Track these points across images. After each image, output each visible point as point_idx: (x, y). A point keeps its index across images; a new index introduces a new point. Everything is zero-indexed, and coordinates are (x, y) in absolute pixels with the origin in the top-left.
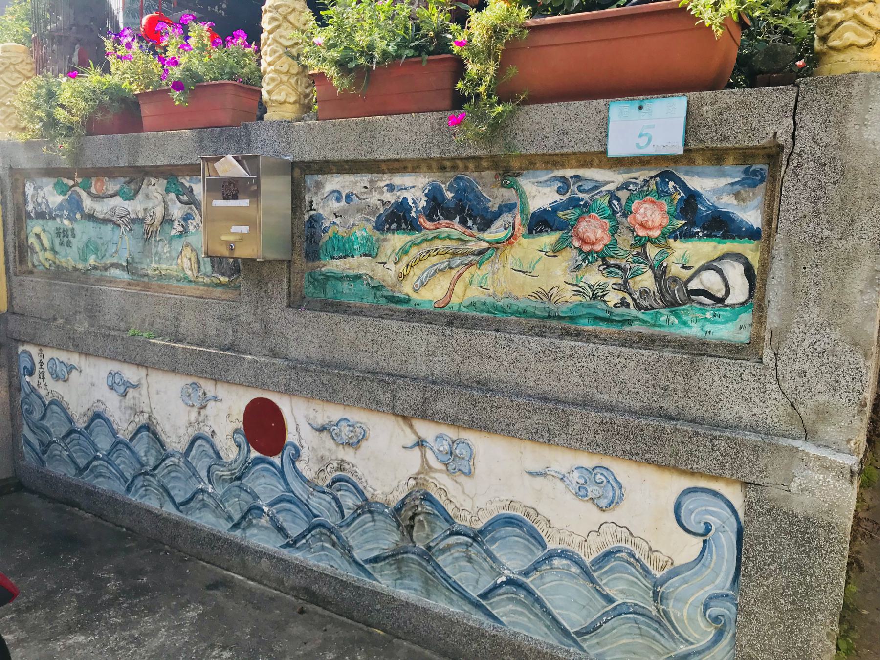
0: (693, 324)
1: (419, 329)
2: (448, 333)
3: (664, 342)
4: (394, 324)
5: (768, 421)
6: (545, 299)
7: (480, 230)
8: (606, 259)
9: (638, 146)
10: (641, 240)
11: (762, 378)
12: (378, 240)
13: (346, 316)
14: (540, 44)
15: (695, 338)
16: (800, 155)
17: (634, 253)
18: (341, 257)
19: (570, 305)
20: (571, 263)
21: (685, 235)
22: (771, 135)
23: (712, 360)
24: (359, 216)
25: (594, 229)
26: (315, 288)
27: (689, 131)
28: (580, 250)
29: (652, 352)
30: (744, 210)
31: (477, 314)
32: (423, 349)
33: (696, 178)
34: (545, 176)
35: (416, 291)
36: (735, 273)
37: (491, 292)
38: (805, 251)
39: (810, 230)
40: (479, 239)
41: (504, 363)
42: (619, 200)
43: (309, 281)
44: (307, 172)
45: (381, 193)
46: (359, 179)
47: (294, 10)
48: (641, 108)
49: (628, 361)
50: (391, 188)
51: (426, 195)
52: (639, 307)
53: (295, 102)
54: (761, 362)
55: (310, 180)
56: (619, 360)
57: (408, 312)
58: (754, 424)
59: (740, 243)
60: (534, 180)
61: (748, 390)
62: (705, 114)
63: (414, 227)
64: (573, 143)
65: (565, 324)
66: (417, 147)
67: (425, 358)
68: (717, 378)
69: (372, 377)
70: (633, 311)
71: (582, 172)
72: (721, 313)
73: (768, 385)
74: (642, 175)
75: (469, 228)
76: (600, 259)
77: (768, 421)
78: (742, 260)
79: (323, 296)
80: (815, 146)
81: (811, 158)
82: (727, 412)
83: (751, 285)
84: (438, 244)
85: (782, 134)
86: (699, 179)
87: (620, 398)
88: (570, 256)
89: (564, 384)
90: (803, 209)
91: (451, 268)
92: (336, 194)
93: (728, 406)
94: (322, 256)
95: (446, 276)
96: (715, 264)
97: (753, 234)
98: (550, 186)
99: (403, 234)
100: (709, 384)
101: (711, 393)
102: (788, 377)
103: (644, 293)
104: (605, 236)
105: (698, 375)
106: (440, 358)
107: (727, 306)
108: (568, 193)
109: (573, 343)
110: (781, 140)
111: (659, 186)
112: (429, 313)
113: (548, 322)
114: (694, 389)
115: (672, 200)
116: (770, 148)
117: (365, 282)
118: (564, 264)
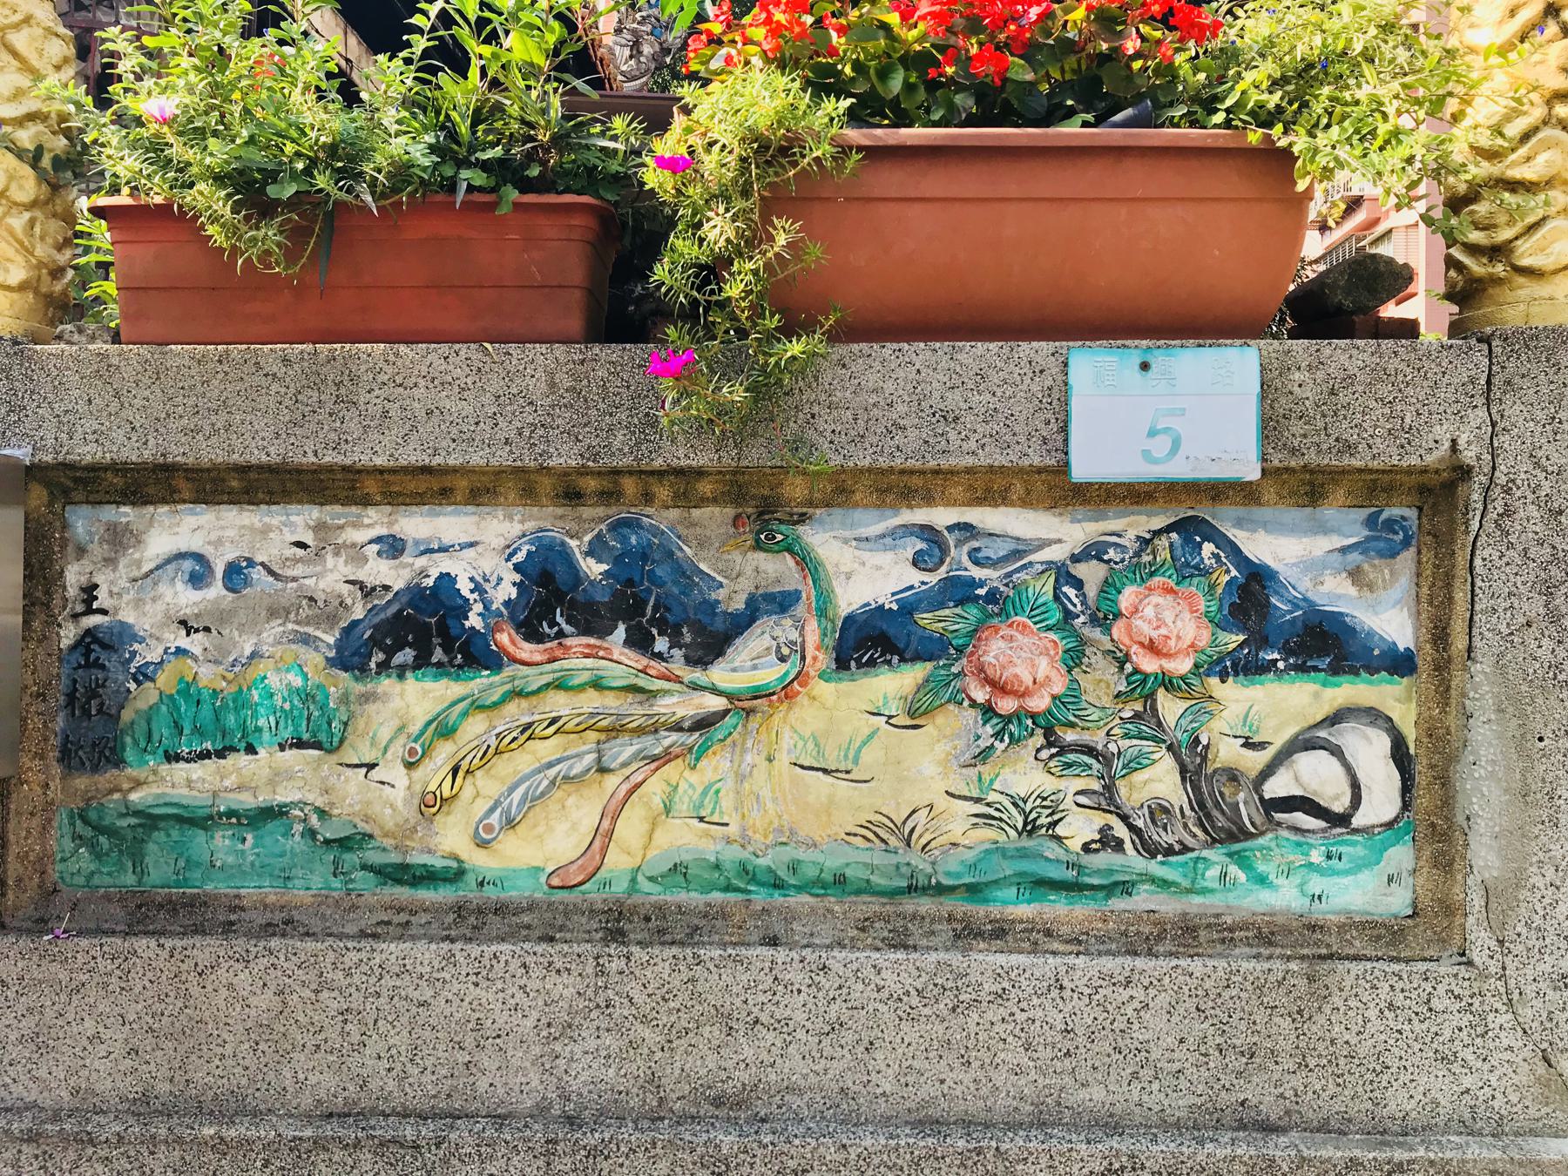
0: (1281, 881)
1: (515, 965)
2: (616, 965)
3: (1226, 934)
4: (425, 953)
5: (1496, 1103)
6: (893, 841)
7: (690, 661)
8: (1051, 734)
9: (1146, 454)
10: (1144, 681)
11: (1476, 1001)
12: (345, 699)
13: (240, 944)
14: (877, 193)
15: (1286, 912)
16: (1508, 491)
17: (1127, 714)
18: (204, 755)
19: (970, 856)
20: (960, 743)
21: (1246, 667)
22: (1447, 445)
23: (1357, 968)
24: (274, 629)
25: (1025, 657)
26: (98, 855)
27: (1270, 427)
28: (988, 710)
29: (1210, 963)
30: (1373, 608)
31: (694, 898)
32: (530, 1022)
33: (1261, 535)
34: (877, 523)
35: (483, 844)
36: (1370, 753)
37: (733, 830)
38: (1540, 701)
39: (1544, 653)
40: (695, 687)
41: (801, 1034)
42: (1078, 584)
43: (76, 837)
44: (78, 495)
45: (363, 559)
46: (275, 521)
47: (27, 20)
48: (1145, 366)
49: (1152, 992)
50: (393, 547)
51: (517, 568)
52: (1150, 850)
53: (22, 287)
54: (1470, 963)
55: (83, 522)
56: (1129, 992)
57: (460, 909)
58: (1467, 1116)
59: (1371, 683)
60: (848, 534)
61: (1447, 1034)
62: (1296, 389)
63: (474, 655)
64: (972, 445)
65: (959, 906)
66: (501, 436)
67: (537, 1050)
68: (1372, 1013)
69: (351, 1134)
70: (1133, 860)
71: (974, 515)
72: (1341, 849)
73: (1491, 1017)
74: (1133, 525)
75: (659, 656)
76: (1039, 731)
77: (1496, 1103)
78: (1380, 722)
79: (129, 879)
80: (1537, 472)
81: (1531, 497)
82: (1404, 1094)
83: (1404, 780)
84: (559, 703)
85: (1469, 443)
86: (1270, 538)
87: (1136, 1093)
88: (955, 726)
89: (980, 1074)
90: (1526, 607)
91: (603, 770)
92: (188, 565)
93: (1404, 1077)
94: (130, 755)
95: (586, 792)
96: (1323, 734)
97: (1400, 664)
98: (893, 548)
99: (436, 677)
100: (1355, 1029)
101: (1362, 1052)
102: (1530, 990)
103: (1160, 811)
104: (1054, 674)
105: (1327, 1009)
106: (592, 1044)
107: (1356, 831)
108: (944, 568)
109: (1001, 959)
110: (1468, 456)
111: (1179, 552)
112: (532, 907)
113: (907, 903)
114: (1321, 1047)
115: (1212, 587)
116: (1437, 472)
117: (298, 828)
118: (942, 748)
